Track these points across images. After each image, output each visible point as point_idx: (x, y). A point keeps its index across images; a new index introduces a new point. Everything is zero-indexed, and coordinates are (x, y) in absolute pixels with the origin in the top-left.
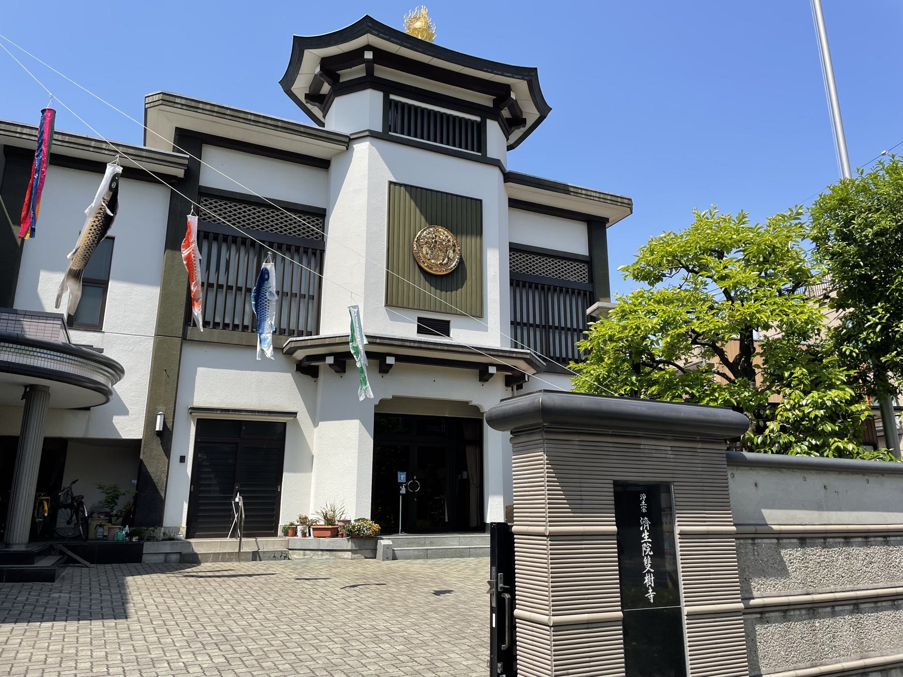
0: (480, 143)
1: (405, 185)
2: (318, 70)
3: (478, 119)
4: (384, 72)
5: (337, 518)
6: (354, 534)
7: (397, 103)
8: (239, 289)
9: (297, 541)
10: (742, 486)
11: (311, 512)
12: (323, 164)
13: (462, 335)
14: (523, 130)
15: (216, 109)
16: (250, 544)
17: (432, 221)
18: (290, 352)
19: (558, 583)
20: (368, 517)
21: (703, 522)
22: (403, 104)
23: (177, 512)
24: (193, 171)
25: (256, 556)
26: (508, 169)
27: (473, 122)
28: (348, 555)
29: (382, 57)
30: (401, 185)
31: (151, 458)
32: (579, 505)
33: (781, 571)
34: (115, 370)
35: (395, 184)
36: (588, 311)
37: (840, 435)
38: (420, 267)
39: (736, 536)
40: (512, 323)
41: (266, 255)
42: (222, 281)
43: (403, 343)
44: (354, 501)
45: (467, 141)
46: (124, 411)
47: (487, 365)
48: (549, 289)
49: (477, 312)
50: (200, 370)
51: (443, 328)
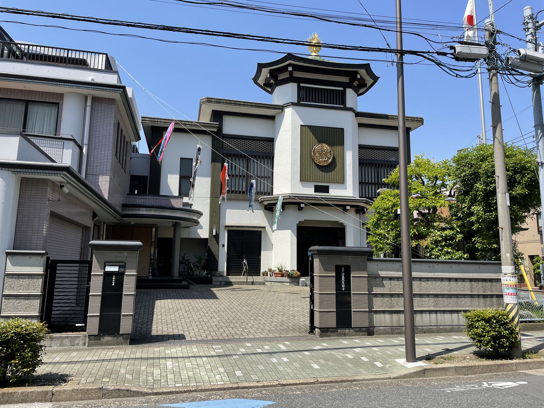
0: (343, 102)
1: (308, 126)
2: (268, 76)
3: (342, 89)
4: (297, 74)
5: (283, 270)
6: (290, 276)
7: (303, 87)
8: (240, 176)
9: (268, 278)
10: (372, 266)
11: (273, 266)
12: (272, 118)
13: (335, 192)
14: (365, 89)
15: (228, 102)
16: (250, 279)
17: (320, 141)
18: (262, 202)
19: (321, 285)
20: (296, 269)
21: (359, 274)
22: (306, 87)
23: (223, 266)
24: (220, 129)
25: (253, 283)
26: (359, 110)
27: (339, 91)
28: (288, 284)
29: (296, 68)
30: (306, 126)
31: (212, 244)
32: (326, 270)
33: (383, 286)
34: (200, 214)
35: (303, 126)
36: (378, 191)
37: (448, 246)
38: (315, 163)
39: (368, 277)
40: (360, 183)
41: (250, 161)
42: (234, 173)
43: (308, 198)
44: (290, 263)
45: (337, 101)
46: (202, 228)
47: (346, 205)
48: (379, 165)
49: (341, 181)
50: (228, 210)
51: (326, 189)
